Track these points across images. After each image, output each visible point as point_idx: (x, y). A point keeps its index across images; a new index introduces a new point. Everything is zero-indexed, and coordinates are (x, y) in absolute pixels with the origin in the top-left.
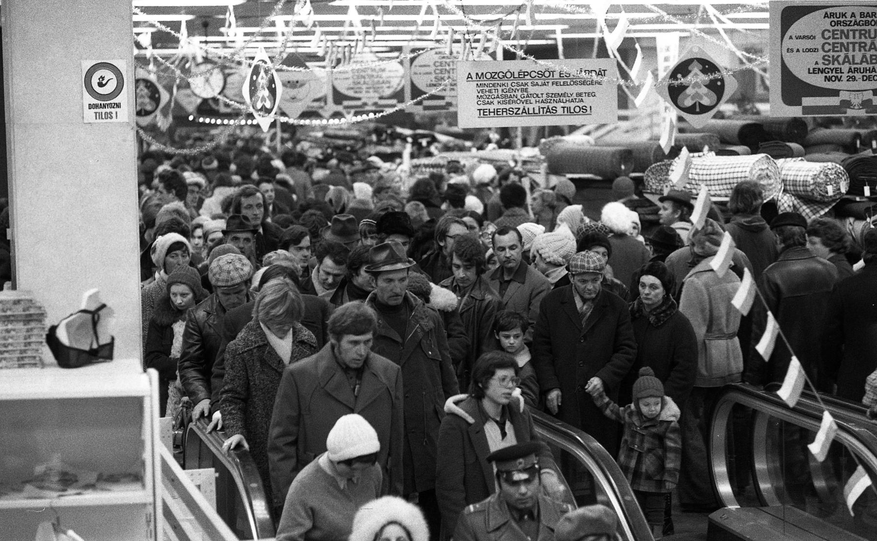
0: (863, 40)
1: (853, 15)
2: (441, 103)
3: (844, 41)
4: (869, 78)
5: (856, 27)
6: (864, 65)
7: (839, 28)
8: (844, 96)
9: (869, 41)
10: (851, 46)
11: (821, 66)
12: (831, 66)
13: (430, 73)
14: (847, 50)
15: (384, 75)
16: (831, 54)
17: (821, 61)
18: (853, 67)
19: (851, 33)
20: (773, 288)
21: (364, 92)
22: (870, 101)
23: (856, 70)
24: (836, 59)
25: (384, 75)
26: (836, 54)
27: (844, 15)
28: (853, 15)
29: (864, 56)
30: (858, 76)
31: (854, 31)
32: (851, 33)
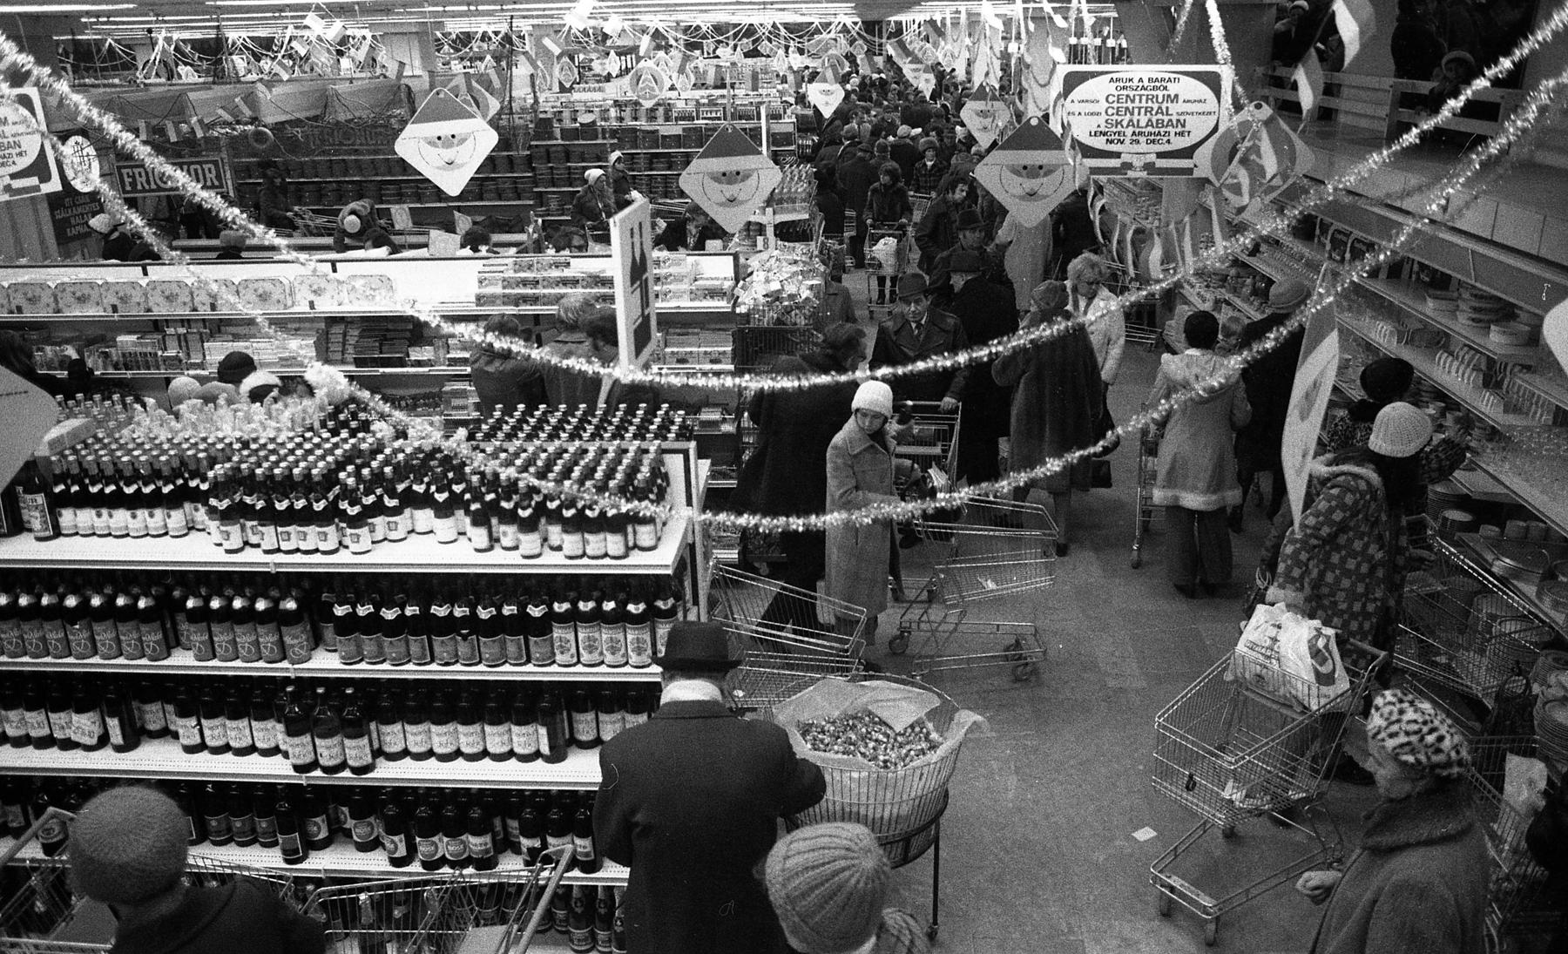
0: (1150, 104)
1: (1141, 80)
2: (1113, 163)
3: (1130, 105)
4: (1153, 142)
5: (1143, 92)
6: (1150, 129)
7: (1125, 92)
8: (1125, 158)
9: (1156, 106)
10: (1136, 111)
11: (1103, 129)
12: (1114, 130)
13: (1098, 114)
14: (1132, 114)
15: (1174, 108)
16: (1115, 117)
17: (1103, 124)
18: (1137, 130)
19: (1137, 98)
20: (638, 259)
21: (1127, 141)
22: (9, 185)
23: (1140, 134)
24: (1118, 123)
25: (1174, 108)
26: (1120, 119)
27: (1131, 80)
28: (1141, 80)
29: (1150, 120)
30: (1142, 139)
31: (1141, 96)
32: (1137, 98)
